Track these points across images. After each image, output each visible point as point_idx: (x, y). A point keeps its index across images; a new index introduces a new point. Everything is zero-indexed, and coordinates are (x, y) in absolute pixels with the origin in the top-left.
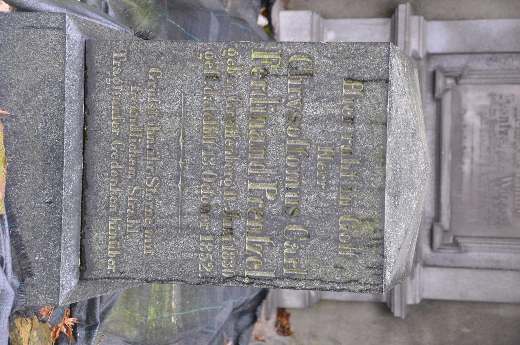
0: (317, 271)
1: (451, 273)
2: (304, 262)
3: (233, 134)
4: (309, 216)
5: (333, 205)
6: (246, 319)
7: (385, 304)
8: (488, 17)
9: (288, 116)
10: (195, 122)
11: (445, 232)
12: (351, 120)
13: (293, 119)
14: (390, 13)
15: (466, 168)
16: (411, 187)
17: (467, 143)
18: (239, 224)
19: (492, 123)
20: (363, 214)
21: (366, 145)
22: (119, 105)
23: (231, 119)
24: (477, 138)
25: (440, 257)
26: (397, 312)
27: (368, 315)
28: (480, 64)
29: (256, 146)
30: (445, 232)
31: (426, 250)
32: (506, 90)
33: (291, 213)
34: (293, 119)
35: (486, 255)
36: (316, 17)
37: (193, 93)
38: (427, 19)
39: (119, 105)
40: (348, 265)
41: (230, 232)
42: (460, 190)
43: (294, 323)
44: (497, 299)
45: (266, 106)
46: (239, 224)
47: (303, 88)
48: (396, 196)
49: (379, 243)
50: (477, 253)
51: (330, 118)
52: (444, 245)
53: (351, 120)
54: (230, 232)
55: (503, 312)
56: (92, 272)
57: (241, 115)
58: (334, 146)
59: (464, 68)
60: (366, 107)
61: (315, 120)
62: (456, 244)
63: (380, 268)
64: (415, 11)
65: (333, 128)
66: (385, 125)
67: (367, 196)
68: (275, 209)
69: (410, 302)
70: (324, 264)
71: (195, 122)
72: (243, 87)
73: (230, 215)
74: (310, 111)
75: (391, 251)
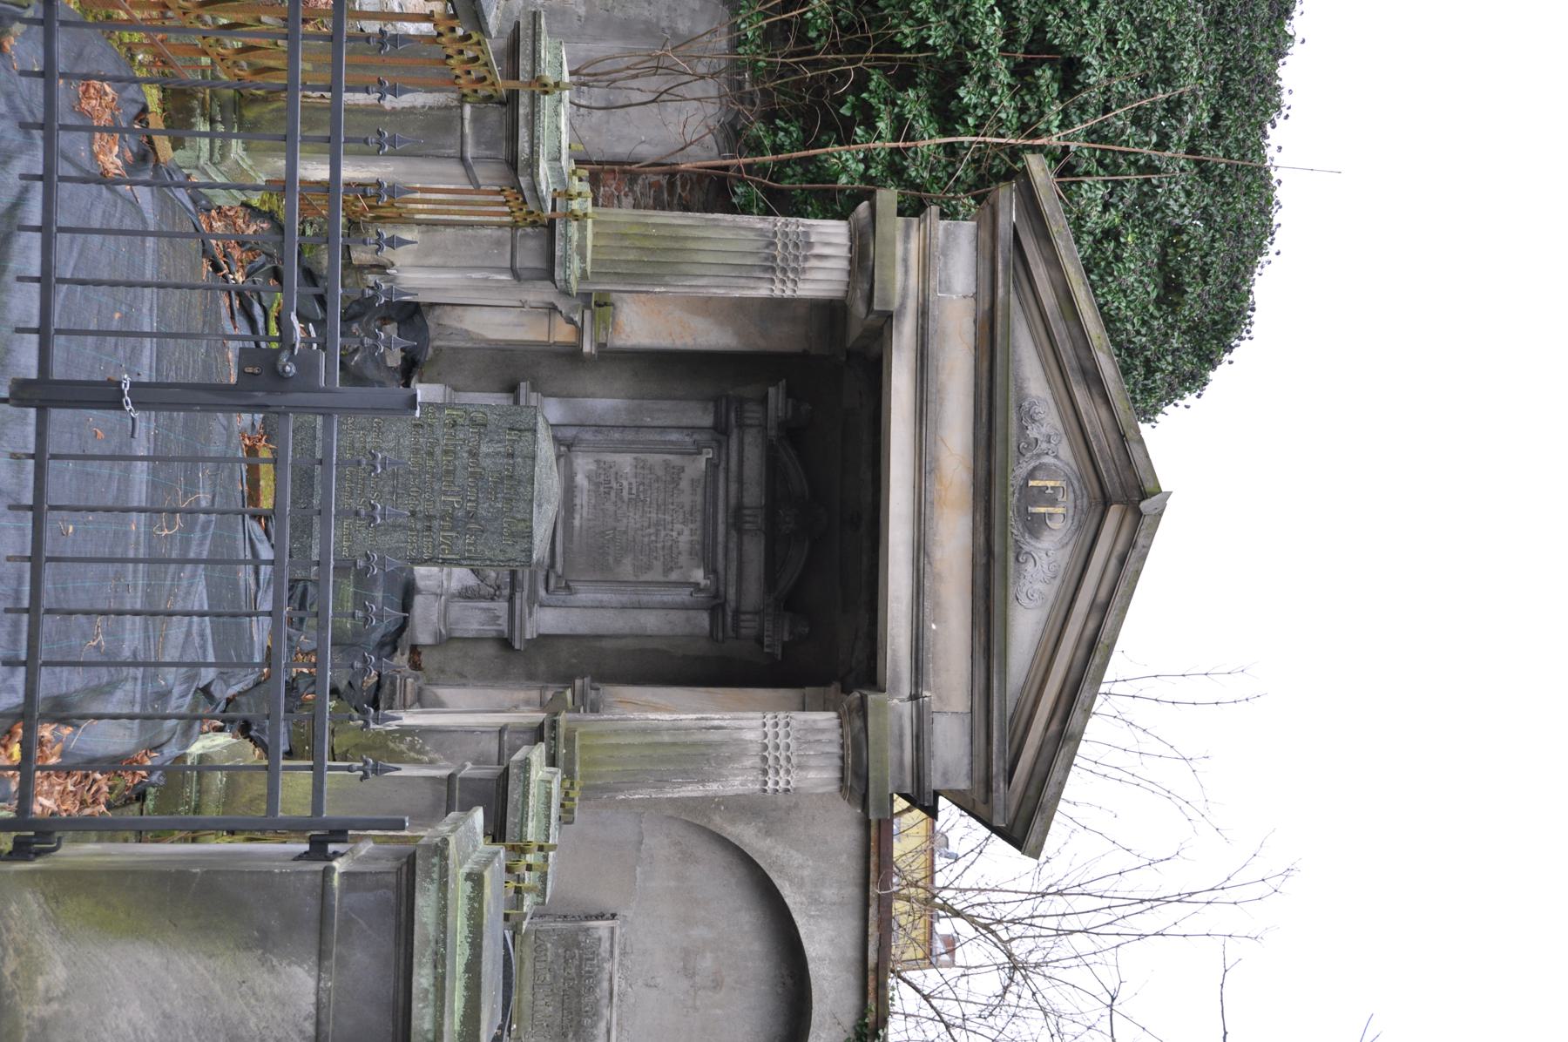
0: (488, 554)
1: (563, 611)
2: (480, 548)
3: (432, 463)
4: (484, 518)
5: (500, 511)
6: (388, 649)
7: (506, 640)
8: (593, 395)
9: (470, 452)
10: (406, 455)
11: (559, 577)
12: (512, 455)
13: (473, 454)
14: (512, 389)
15: (577, 522)
16: (549, 502)
17: (577, 501)
18: (436, 523)
19: (598, 485)
20: (519, 516)
21: (521, 471)
22: (352, 443)
23: (431, 454)
24: (585, 497)
25: (553, 599)
26: (517, 646)
27: (490, 650)
28: (588, 435)
29: (448, 472)
30: (559, 577)
31: (542, 593)
32: (609, 457)
33: (471, 516)
34: (473, 454)
35: (591, 596)
36: (448, 390)
37: (404, 436)
38: (544, 395)
39: (352, 443)
40: (509, 550)
41: (429, 528)
42: (571, 541)
43: (425, 659)
44: (600, 632)
45: (455, 446)
46: (436, 523)
47: (480, 434)
48: (540, 506)
49: (530, 535)
50: (585, 595)
51: (498, 453)
52: (557, 588)
53: (512, 455)
54: (429, 528)
55: (604, 644)
56: (1080, 78)
57: (438, 451)
58: (500, 472)
59: (575, 437)
60: (522, 446)
61: (488, 455)
62: (568, 587)
63: (530, 551)
64: (534, 388)
65: (499, 460)
66: (534, 458)
67: (522, 505)
68: (460, 514)
69: (528, 637)
70: (492, 549)
71: (406, 455)
72: (439, 433)
73: (429, 518)
74: (484, 449)
75: (537, 541)
